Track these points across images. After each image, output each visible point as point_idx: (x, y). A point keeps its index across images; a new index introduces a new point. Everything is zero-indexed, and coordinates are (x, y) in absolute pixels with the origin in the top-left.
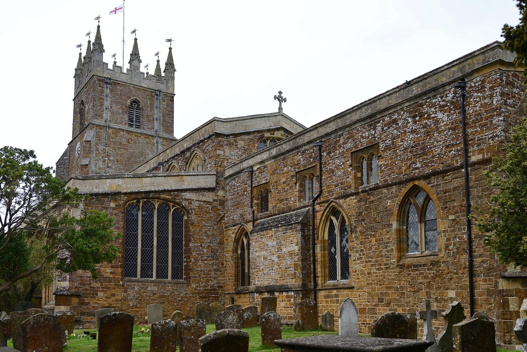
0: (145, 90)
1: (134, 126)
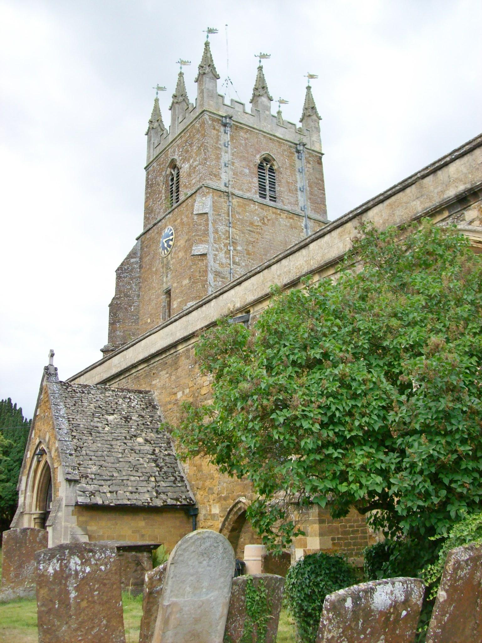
0: (280, 141)
1: (268, 198)
